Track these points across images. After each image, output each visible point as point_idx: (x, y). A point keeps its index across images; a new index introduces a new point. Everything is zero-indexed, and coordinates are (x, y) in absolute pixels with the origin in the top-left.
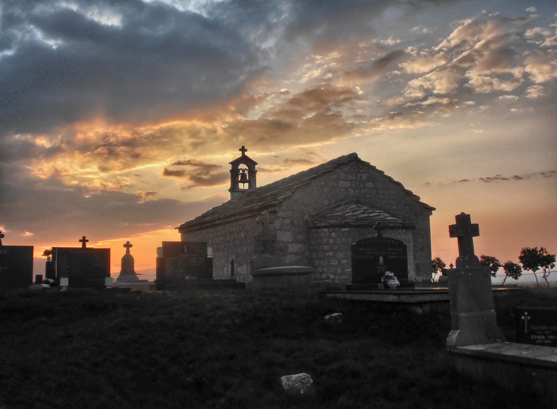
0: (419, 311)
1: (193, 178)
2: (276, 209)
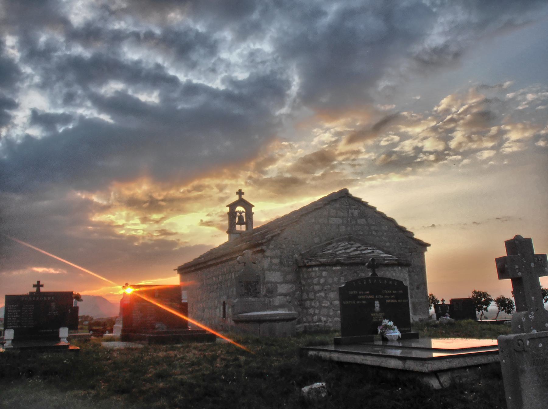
0: (435, 383)
2: (264, 247)
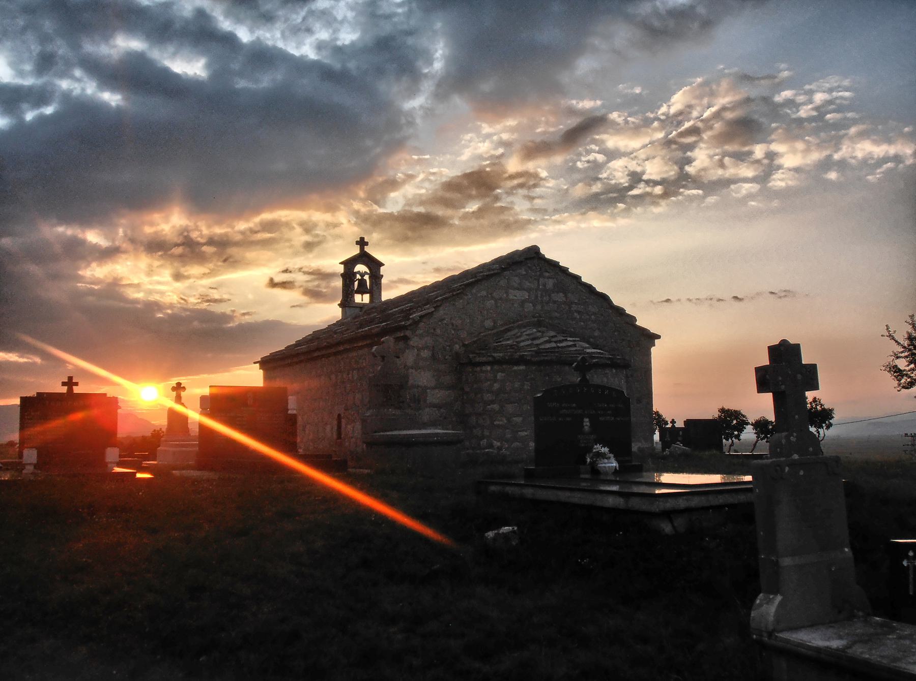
0: (667, 528)
1: (309, 292)
2: (408, 333)
